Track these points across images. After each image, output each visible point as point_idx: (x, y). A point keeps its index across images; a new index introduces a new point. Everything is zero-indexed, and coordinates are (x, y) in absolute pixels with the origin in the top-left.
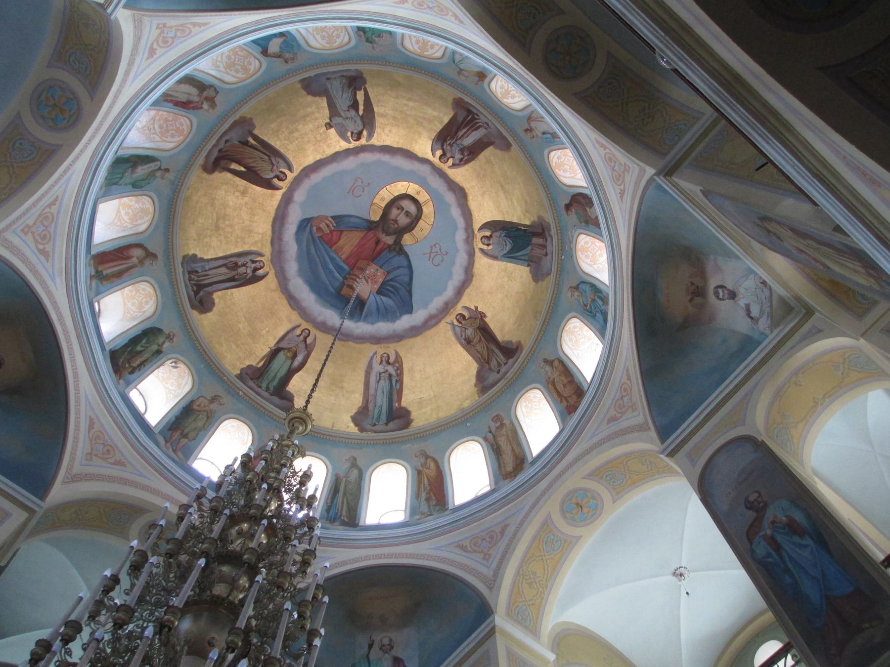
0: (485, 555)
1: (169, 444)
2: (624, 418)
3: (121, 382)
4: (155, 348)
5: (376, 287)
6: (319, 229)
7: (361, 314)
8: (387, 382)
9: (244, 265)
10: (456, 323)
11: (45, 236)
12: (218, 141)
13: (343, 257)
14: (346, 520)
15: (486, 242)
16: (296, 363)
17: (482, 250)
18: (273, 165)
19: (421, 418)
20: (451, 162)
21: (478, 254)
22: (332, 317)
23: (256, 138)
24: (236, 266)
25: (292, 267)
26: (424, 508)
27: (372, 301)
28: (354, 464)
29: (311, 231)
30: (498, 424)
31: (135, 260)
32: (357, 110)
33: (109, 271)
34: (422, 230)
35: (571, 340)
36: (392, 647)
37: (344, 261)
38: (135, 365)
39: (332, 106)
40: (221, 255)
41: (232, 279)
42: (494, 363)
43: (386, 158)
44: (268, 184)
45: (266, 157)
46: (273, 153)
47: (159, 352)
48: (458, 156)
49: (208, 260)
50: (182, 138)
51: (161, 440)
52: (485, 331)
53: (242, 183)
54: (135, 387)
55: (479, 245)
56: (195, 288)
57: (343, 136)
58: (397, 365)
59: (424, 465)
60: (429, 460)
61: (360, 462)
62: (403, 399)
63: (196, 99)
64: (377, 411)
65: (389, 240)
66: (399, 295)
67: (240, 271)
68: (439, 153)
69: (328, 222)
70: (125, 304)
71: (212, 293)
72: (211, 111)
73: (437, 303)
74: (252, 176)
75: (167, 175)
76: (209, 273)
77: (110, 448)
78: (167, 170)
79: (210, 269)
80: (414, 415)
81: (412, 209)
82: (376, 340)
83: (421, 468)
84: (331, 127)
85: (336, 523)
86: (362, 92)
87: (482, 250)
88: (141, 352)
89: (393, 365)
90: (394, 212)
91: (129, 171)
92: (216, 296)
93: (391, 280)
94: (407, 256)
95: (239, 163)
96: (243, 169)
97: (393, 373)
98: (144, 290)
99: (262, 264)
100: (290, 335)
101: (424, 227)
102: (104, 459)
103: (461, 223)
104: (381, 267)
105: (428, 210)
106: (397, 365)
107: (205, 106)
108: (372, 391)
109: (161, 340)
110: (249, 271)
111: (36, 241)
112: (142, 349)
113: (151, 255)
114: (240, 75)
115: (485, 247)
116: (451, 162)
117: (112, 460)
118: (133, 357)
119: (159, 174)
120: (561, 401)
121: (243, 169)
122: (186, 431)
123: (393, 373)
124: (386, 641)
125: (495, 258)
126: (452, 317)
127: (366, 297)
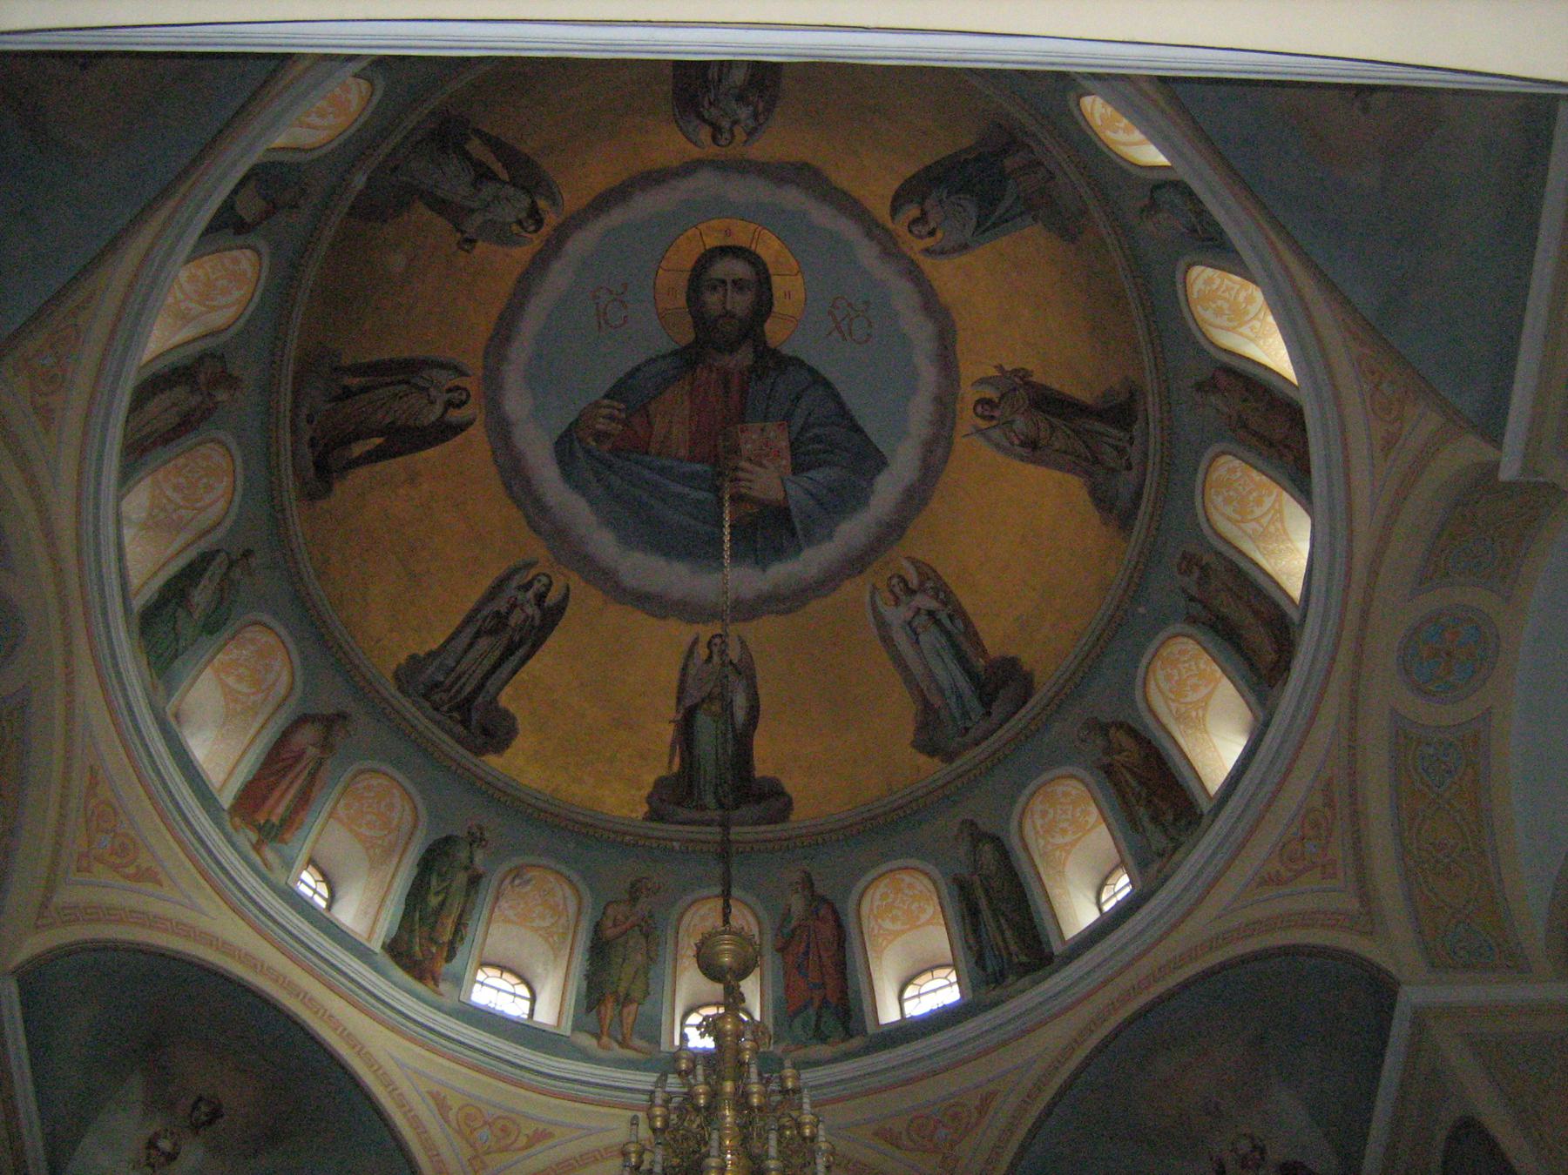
0: (945, 1158)
1: (605, 1039)
2: (1407, 427)
3: (443, 987)
4: (462, 878)
5: (785, 462)
6: (600, 436)
7: (794, 534)
8: (934, 629)
9: (513, 606)
10: (983, 424)
11: (123, 845)
12: (295, 430)
13: (683, 452)
14: (1024, 959)
15: (924, 230)
16: (740, 715)
17: (927, 251)
18: (426, 389)
19: (1045, 654)
20: (740, 135)
21: (927, 264)
22: (744, 579)
23: (356, 370)
24: (501, 619)
25: (604, 544)
26: (1158, 841)
27: (797, 493)
28: (976, 835)
29: (588, 452)
30: (1196, 573)
31: (312, 751)
32: (491, 176)
33: (281, 809)
34: (788, 295)
35: (1219, 312)
36: (1263, 1151)
37: (692, 459)
38: (447, 937)
39: (441, 206)
40: (457, 620)
41: (509, 651)
42: (1109, 455)
43: (616, 216)
44: (445, 431)
45: (404, 387)
46: (408, 370)
47: (475, 881)
48: (744, 113)
49: (443, 647)
50: (226, 481)
51: (586, 1041)
52: (1048, 402)
53: (393, 467)
54: (475, 981)
55: (915, 246)
56: (456, 715)
57: (503, 237)
58: (929, 584)
59: (1108, 751)
60: (1112, 731)
61: (985, 825)
62: (987, 643)
63: (195, 400)
64: (953, 702)
65: (744, 357)
66: (838, 447)
67: (515, 626)
68: (705, 133)
69: (606, 412)
70: (357, 835)
71: (494, 700)
72: (238, 394)
73: (920, 412)
74: (406, 439)
75: (254, 562)
76: (460, 669)
77: (502, 1122)
78: (247, 554)
79: (458, 663)
80: (1027, 659)
81: (739, 269)
82: (856, 564)
83: (1106, 760)
84: (472, 241)
85: (1011, 978)
86: (476, 141)
87: (927, 251)
88: (443, 903)
89: (922, 588)
90: (712, 300)
91: (181, 614)
92: (504, 700)
93: (803, 429)
94: (798, 363)
95: (358, 437)
96: (377, 441)
97: (934, 605)
98: (369, 788)
99: (544, 580)
100: (692, 671)
101: (788, 288)
102: (506, 1149)
103: (849, 230)
104: (766, 419)
105: (769, 248)
106: (929, 584)
107: (222, 396)
108: (917, 669)
109: (463, 855)
110: (531, 610)
111: (116, 868)
112: (440, 898)
113: (333, 722)
114: (237, 294)
115: (929, 242)
116: (740, 135)
117: (523, 1141)
118: (433, 928)
119: (236, 573)
120: (1281, 456)
121: (377, 441)
122: (622, 990)
123: (934, 605)
124: (1245, 1146)
125: (964, 247)
126: (967, 418)
127: (780, 496)
